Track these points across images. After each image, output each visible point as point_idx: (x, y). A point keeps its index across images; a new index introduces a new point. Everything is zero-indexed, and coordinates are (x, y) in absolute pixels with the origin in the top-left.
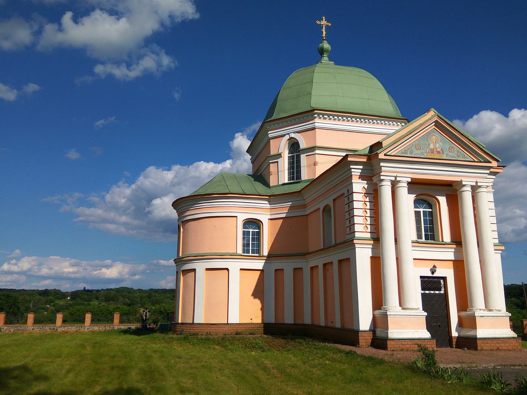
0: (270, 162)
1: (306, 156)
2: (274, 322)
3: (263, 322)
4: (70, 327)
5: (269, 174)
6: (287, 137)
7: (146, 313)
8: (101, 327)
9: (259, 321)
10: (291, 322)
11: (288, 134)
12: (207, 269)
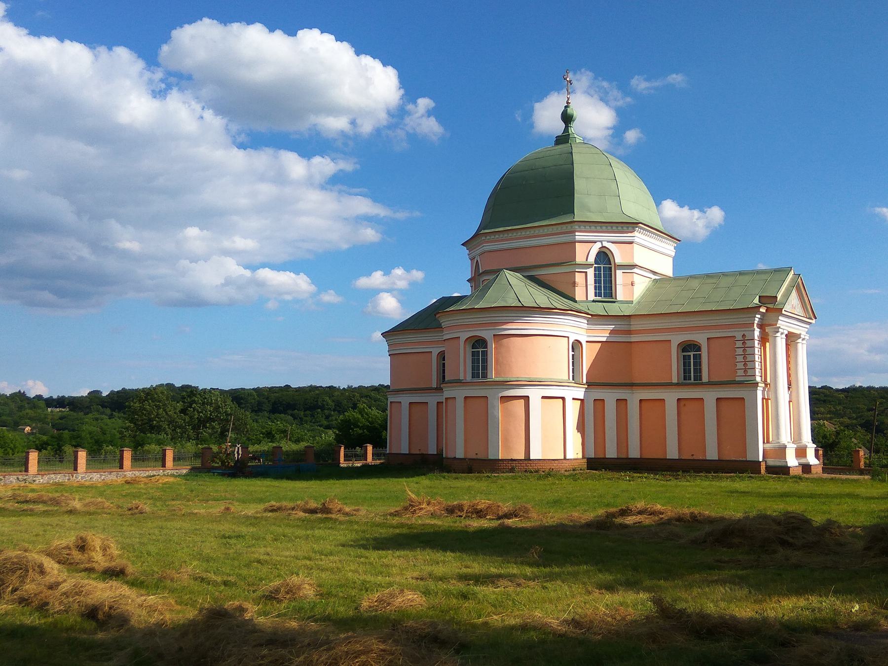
0: (577, 270)
1: (623, 273)
2: (639, 457)
3: (583, 457)
4: (53, 476)
5: (574, 284)
6: (599, 245)
7: (238, 448)
8: (104, 474)
9: (580, 456)
10: (715, 457)
11: (601, 242)
12: (543, 397)
